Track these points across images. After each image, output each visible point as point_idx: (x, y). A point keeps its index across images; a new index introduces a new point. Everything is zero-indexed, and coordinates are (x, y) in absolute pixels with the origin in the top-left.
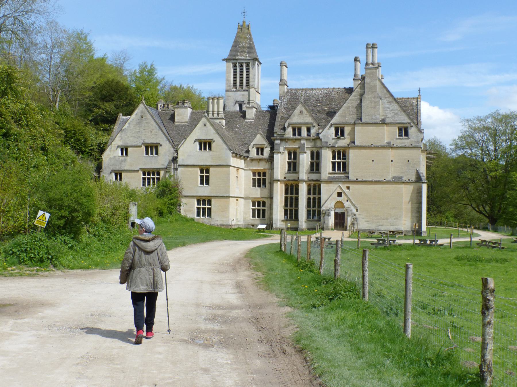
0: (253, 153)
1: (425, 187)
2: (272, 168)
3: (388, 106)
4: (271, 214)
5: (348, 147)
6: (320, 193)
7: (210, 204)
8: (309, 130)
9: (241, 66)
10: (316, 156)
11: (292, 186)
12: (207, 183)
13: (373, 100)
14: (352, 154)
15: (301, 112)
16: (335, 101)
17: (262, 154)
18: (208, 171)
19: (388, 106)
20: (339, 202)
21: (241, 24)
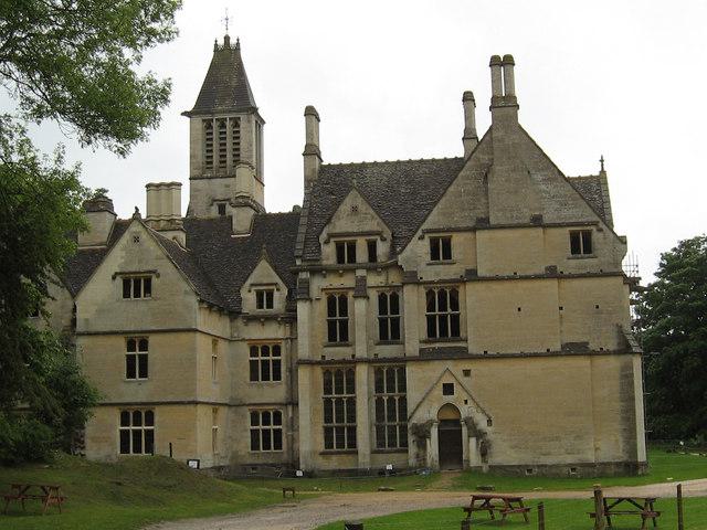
0: (249, 301)
1: (637, 362)
2: (293, 339)
3: (543, 187)
4: (293, 440)
5: (462, 281)
6: (403, 388)
7: (150, 421)
8: (372, 247)
9: (223, 126)
10: (389, 305)
11: (339, 374)
12: (144, 374)
13: (513, 175)
14: (470, 296)
15: (355, 209)
16: (426, 187)
17: (270, 305)
18: (144, 345)
19: (543, 187)
20: (449, 406)
21: (221, 42)
